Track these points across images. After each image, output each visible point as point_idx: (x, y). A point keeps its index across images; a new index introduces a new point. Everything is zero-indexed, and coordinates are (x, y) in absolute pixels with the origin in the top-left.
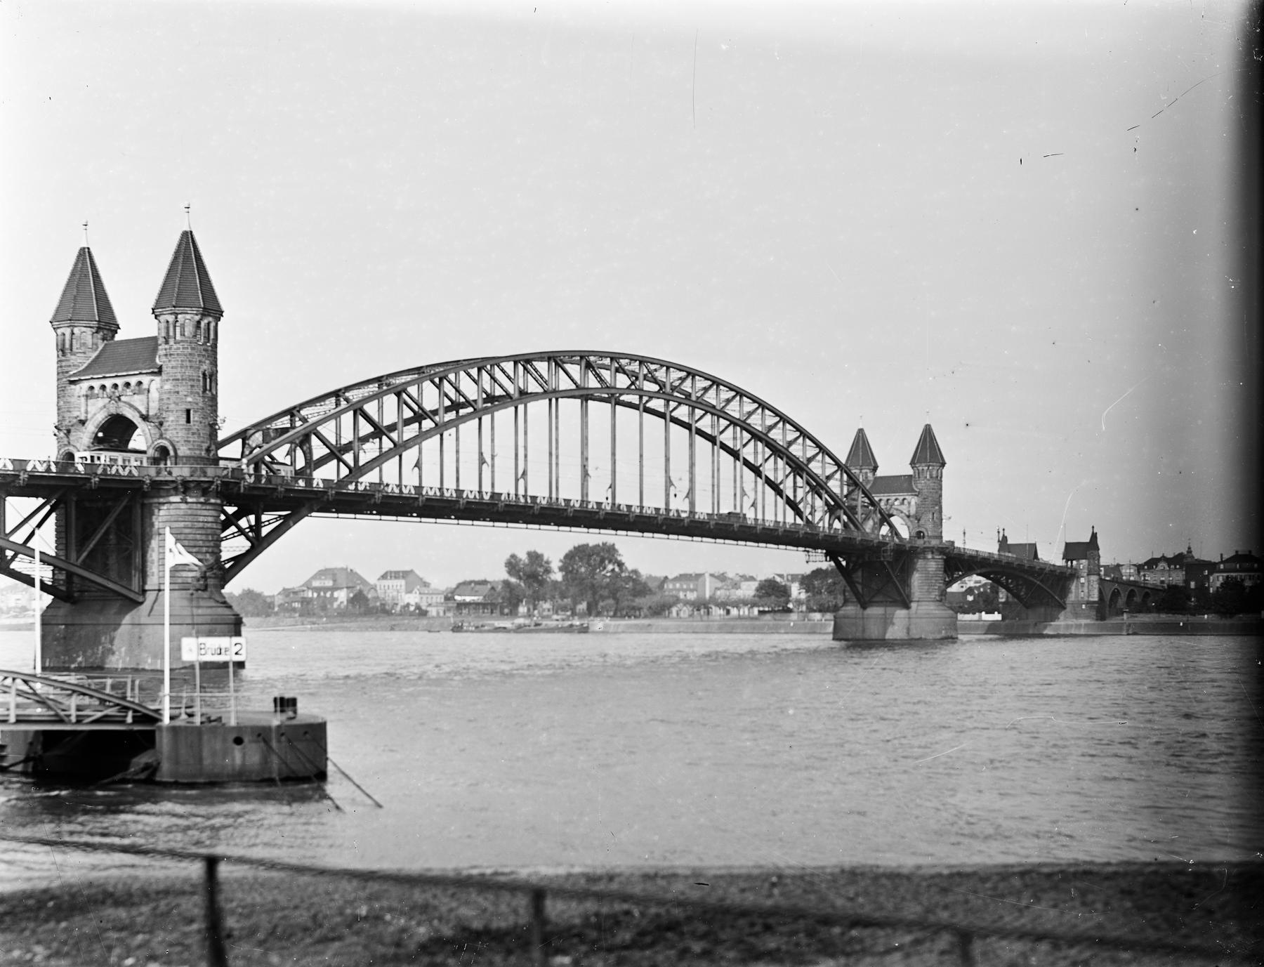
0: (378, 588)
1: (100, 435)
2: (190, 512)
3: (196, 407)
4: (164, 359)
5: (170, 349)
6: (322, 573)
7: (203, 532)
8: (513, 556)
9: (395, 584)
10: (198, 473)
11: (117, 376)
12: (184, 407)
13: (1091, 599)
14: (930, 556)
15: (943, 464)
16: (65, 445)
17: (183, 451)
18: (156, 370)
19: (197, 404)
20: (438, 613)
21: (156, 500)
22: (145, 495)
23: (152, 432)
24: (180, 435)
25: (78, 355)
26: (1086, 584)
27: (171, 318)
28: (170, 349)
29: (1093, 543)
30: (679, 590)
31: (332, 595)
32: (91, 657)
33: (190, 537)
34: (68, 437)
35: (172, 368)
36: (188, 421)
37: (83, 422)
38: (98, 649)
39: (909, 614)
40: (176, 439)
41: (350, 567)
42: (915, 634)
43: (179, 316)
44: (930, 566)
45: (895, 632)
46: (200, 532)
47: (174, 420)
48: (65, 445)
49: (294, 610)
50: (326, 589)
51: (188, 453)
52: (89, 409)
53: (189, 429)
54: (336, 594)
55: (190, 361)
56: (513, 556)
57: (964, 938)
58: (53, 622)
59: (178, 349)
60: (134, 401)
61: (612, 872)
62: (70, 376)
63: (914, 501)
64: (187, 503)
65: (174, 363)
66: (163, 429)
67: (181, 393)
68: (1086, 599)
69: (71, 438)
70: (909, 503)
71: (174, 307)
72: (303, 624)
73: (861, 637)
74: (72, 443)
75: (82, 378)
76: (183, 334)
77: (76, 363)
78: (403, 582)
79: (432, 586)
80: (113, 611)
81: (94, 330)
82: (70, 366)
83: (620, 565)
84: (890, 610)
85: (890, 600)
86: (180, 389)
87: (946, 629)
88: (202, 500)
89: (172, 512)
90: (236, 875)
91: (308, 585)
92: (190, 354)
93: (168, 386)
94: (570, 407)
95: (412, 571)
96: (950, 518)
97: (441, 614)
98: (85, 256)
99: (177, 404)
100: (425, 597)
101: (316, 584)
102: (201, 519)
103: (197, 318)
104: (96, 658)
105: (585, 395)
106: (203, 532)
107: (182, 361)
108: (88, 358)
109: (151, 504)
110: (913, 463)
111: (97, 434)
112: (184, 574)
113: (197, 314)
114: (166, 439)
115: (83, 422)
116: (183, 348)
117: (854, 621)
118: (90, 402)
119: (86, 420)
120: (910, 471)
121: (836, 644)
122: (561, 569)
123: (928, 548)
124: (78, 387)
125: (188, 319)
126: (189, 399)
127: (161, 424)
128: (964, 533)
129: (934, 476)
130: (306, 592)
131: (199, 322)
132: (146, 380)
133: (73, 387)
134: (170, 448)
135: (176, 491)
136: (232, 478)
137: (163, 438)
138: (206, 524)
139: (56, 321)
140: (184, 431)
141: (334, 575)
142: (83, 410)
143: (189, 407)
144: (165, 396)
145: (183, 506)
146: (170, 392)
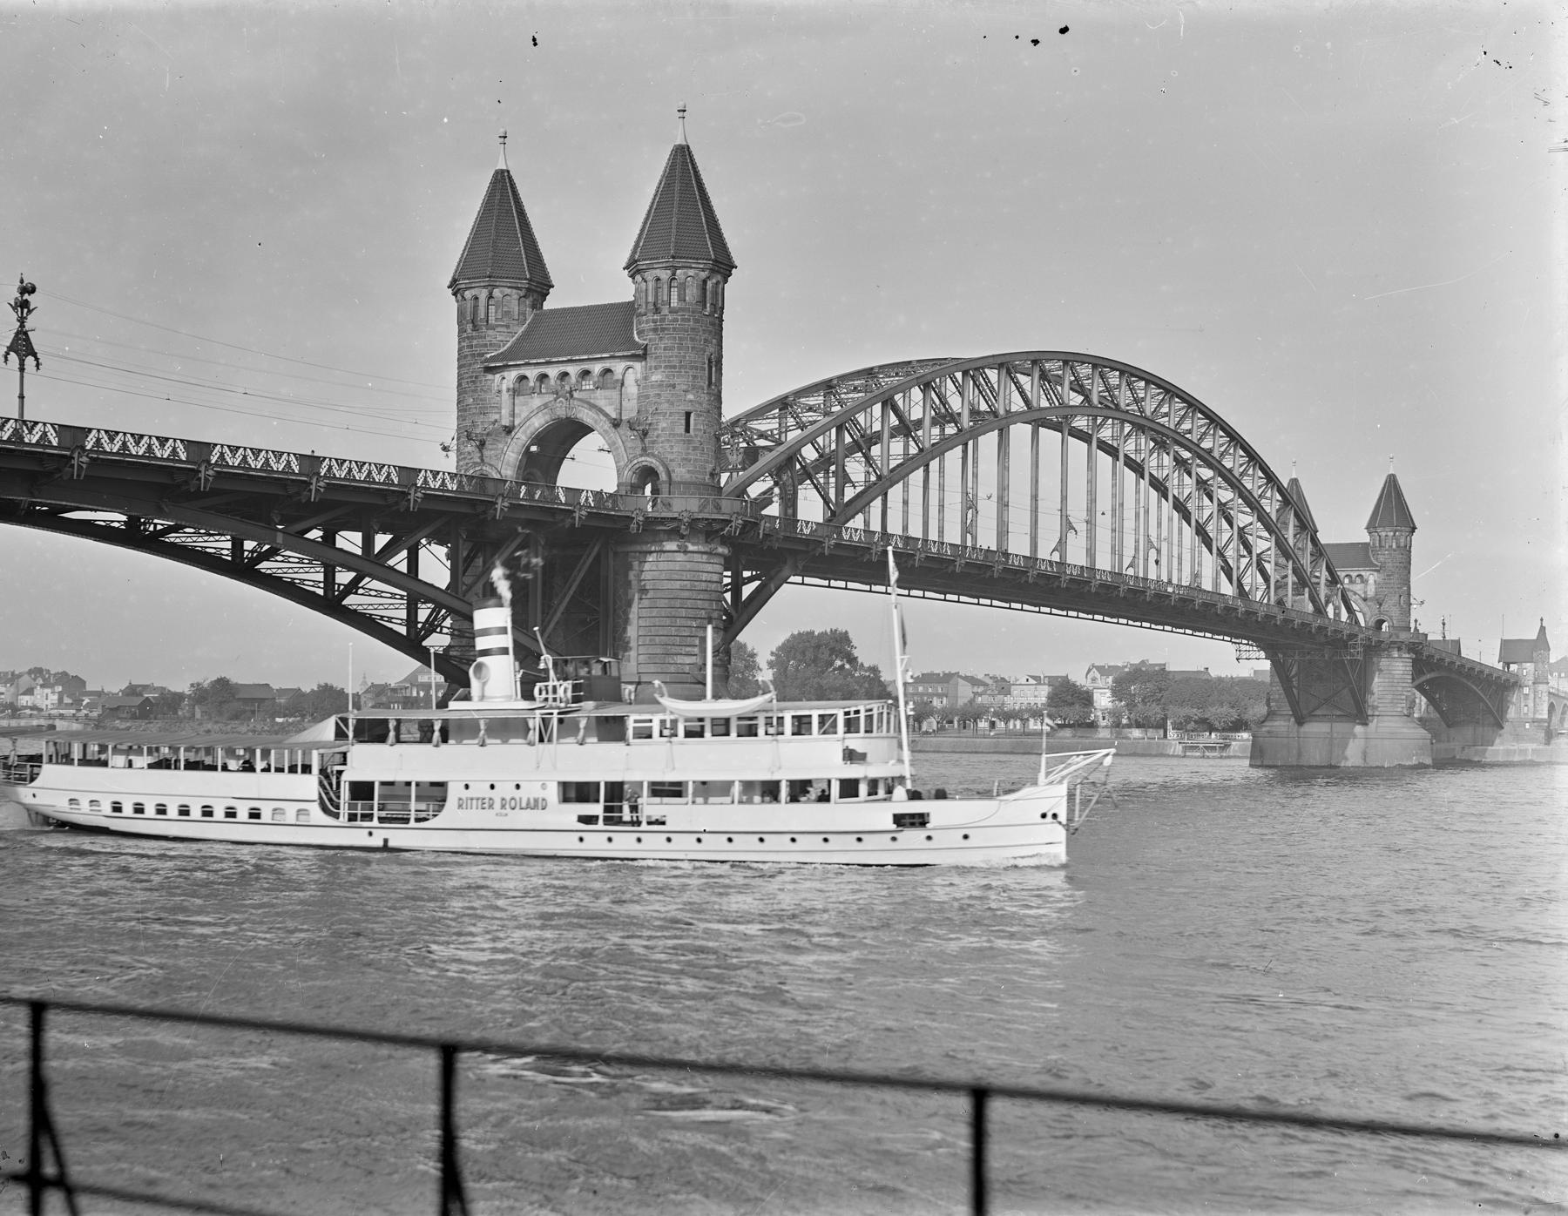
1: (534, 449)
2: (689, 566)
3: (699, 408)
4: (651, 335)
5: (662, 320)
7: (706, 596)
10: (710, 506)
11: (588, 359)
12: (684, 408)
14: (1396, 654)
15: (1414, 529)
16: (475, 464)
17: (680, 473)
18: (641, 352)
19: (701, 404)
21: (638, 548)
22: (636, 539)
23: (629, 445)
24: (675, 450)
25: (499, 329)
26: (1532, 696)
27: (665, 275)
28: (662, 320)
30: (932, 695)
33: (689, 603)
34: (481, 451)
35: (665, 349)
36: (687, 430)
37: (509, 430)
39: (1366, 733)
40: (670, 457)
42: (1373, 762)
45: (1352, 756)
46: (701, 597)
47: (666, 425)
48: (475, 464)
51: (687, 477)
53: (689, 442)
55: (692, 340)
60: (595, 398)
61: (983, 1083)
62: (487, 360)
63: (1372, 578)
64: (686, 552)
66: (646, 440)
67: (678, 387)
68: (1531, 715)
69: (486, 453)
71: (673, 257)
73: (1295, 764)
74: (486, 460)
75: (617, 354)
76: (682, 299)
77: (494, 341)
81: (522, 293)
82: (486, 345)
83: (852, 660)
84: (1341, 727)
85: (1339, 713)
86: (677, 381)
87: (1417, 754)
89: (662, 566)
90: (254, 1059)
92: (693, 329)
93: (656, 377)
94: (1020, 433)
96: (1422, 603)
102: (704, 577)
103: (703, 275)
105: (1039, 421)
106: (706, 596)
110: (1371, 527)
111: (528, 448)
112: (679, 659)
113: (703, 270)
115: (509, 430)
116: (682, 320)
117: (1285, 740)
119: (514, 427)
120: (1366, 538)
121: (1257, 773)
122: (771, 665)
123: (1395, 643)
125: (691, 275)
126: (690, 397)
127: (645, 433)
128: (1444, 624)
129: (1402, 544)
130: (408, 691)
131: (705, 282)
132: (618, 367)
133: (490, 376)
134: (661, 470)
135: (675, 534)
136: (751, 517)
137: (648, 455)
138: (710, 584)
139: (455, 287)
142: (505, 412)
143: (689, 408)
144: (652, 392)
145: (680, 557)
146: (660, 386)
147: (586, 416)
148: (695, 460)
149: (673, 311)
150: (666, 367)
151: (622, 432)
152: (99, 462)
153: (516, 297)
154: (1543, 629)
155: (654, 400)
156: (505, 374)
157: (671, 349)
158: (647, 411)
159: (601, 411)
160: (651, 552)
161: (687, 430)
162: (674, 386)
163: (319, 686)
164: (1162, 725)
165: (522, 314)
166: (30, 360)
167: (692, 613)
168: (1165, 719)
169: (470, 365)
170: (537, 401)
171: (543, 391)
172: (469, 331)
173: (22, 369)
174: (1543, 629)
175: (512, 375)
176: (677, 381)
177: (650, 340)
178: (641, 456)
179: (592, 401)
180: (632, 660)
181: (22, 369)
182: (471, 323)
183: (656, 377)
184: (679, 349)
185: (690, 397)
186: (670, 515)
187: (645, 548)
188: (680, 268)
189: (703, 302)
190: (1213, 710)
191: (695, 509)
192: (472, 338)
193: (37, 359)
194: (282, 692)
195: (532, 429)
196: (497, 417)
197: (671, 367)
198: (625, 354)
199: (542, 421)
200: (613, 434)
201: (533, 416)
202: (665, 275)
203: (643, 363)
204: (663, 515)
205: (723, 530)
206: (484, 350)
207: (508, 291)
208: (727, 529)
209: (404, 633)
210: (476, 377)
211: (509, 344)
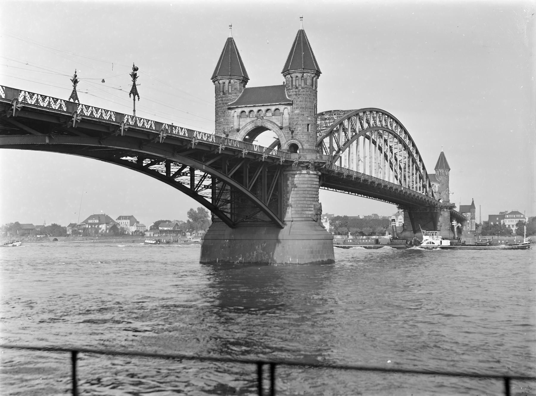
0: (120, 224)
1: (247, 137)
2: (310, 179)
4: (294, 97)
5: (299, 91)
6: (92, 217)
8: (191, 210)
9: (125, 222)
11: (271, 105)
12: (307, 123)
13: (472, 230)
14: (445, 210)
20: (150, 235)
21: (292, 172)
23: (286, 136)
24: (304, 137)
25: (233, 94)
26: (470, 223)
27: (300, 75)
29: (473, 206)
31: (98, 227)
32: (249, 257)
33: (310, 192)
35: (300, 101)
37: (238, 130)
38: (253, 253)
40: (302, 140)
41: (106, 214)
43: (305, 74)
44: (446, 214)
49: (80, 233)
50: (95, 224)
51: (308, 147)
52: (241, 123)
54: (100, 226)
56: (191, 210)
57: (507, 380)
58: (220, 238)
59: (304, 91)
62: (229, 105)
64: (309, 174)
65: (301, 99)
66: (293, 134)
67: (305, 115)
68: (470, 229)
70: (435, 186)
71: (304, 69)
72: (87, 240)
75: (248, 106)
77: (231, 99)
78: (128, 221)
79: (140, 223)
80: (263, 232)
81: (241, 81)
82: (228, 100)
86: (304, 113)
88: (315, 173)
89: (300, 179)
91: (86, 222)
93: (297, 111)
95: (132, 216)
97: (152, 235)
98: (230, 42)
99: (303, 121)
100: (139, 228)
101: (90, 221)
103: (313, 75)
104: (252, 258)
107: (306, 98)
108: (238, 96)
109: (287, 174)
112: (307, 212)
113: (313, 74)
114: (296, 139)
115: (238, 130)
118: (241, 120)
124: (233, 111)
126: (309, 119)
132: (281, 108)
133: (230, 111)
135: (307, 168)
137: (294, 139)
139: (214, 78)
140: (306, 136)
141: (99, 217)
145: (307, 176)
146: (298, 115)
147: (268, 125)
148: (311, 141)
149: (302, 88)
150: (300, 108)
151: (283, 131)
152: (172, 138)
153: (239, 83)
154: (473, 202)
155: (296, 120)
156: (236, 110)
157: (303, 101)
158: (293, 124)
159: (275, 123)
160: (296, 174)
161: (308, 131)
162: (303, 115)
163: (52, 224)
164: (346, 234)
165: (240, 89)
166: (136, 97)
167: (311, 196)
168: (348, 233)
169: (222, 107)
170: (249, 120)
171: (251, 116)
172: (221, 95)
173: (134, 100)
174: (473, 202)
175: (240, 110)
176: (304, 113)
177: (294, 98)
178: (291, 139)
179: (271, 120)
180: (289, 212)
181: (134, 100)
182: (220, 92)
183: (297, 111)
184: (305, 101)
185: (309, 119)
186: (306, 161)
187: (294, 172)
188: (305, 73)
189: (312, 85)
190: (365, 229)
191: (315, 159)
192: (223, 97)
193: (138, 96)
194: (37, 226)
195: (247, 130)
196: (232, 126)
197: (302, 108)
198: (285, 103)
199: (251, 127)
200: (280, 132)
201: (247, 124)
202: (300, 75)
203: (291, 106)
204: (304, 161)
205: (322, 166)
206: (227, 102)
207: (236, 81)
208: (324, 166)
209: (211, 202)
210: (225, 111)
211: (236, 100)
